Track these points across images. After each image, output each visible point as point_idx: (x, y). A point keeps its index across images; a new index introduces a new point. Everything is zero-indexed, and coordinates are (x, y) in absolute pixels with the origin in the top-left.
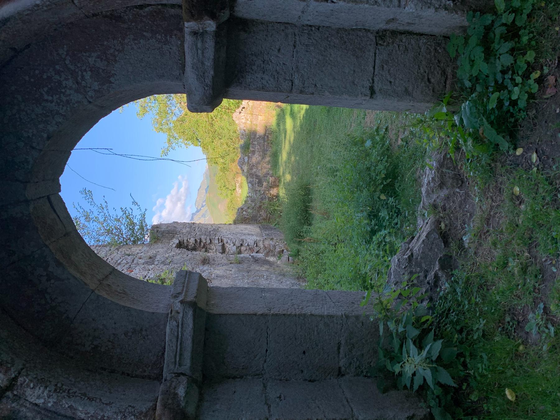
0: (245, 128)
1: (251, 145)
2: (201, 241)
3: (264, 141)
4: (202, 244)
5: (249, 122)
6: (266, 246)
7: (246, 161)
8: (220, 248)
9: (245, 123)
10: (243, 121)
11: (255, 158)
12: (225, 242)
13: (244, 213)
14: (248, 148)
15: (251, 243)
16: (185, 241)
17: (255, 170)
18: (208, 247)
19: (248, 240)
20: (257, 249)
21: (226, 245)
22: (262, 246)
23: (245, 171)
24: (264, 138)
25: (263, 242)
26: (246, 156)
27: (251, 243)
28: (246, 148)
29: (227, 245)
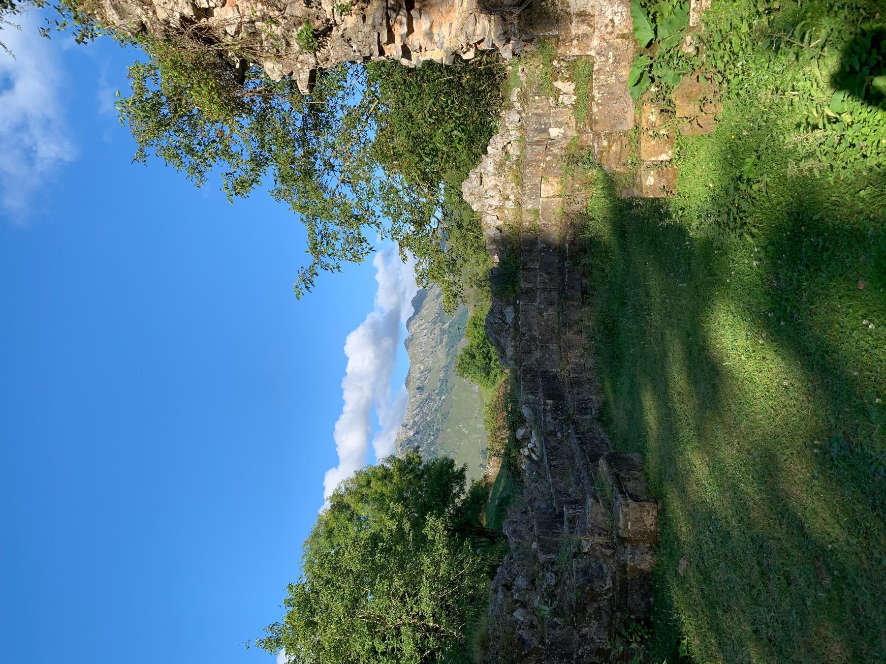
1: (521, 274)
7: (510, 319)
13: (519, 614)
14: (514, 283)
17: (537, 354)
26: (509, 304)
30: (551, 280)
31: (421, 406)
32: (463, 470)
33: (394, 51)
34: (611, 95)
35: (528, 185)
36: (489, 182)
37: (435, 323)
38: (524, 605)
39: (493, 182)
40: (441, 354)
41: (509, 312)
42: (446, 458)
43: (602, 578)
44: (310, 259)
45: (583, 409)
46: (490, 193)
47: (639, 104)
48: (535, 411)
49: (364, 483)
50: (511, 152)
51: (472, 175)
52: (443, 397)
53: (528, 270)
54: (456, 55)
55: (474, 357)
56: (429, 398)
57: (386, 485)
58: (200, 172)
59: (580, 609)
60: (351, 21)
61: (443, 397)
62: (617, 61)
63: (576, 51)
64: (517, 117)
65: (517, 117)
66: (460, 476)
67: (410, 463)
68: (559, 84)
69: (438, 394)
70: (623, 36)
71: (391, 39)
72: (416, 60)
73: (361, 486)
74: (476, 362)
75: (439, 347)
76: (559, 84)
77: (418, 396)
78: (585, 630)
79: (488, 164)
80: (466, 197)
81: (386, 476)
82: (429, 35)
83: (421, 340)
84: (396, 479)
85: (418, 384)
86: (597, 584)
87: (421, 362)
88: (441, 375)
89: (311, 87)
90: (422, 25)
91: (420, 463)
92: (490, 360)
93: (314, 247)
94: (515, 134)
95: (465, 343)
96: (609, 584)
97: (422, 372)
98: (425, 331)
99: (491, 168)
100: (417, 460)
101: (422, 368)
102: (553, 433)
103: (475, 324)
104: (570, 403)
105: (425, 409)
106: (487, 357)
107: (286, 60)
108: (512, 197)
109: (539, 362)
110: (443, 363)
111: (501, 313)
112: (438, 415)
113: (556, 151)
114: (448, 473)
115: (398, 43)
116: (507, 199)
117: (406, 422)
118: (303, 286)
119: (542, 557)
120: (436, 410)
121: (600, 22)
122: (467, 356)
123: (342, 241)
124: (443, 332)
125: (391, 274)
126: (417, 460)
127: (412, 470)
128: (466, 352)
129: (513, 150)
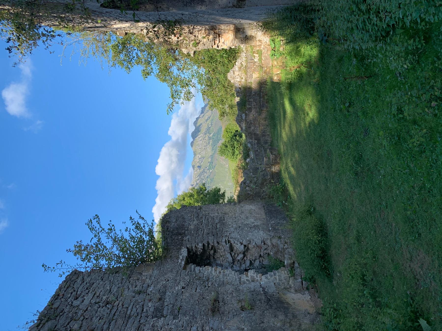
0: (240, 86)
1: (247, 103)
2: (208, 244)
3: (260, 98)
4: (210, 247)
5: (243, 80)
6: (274, 243)
7: (244, 118)
8: (228, 249)
9: (240, 82)
10: (238, 80)
11: (253, 115)
12: (232, 242)
13: (247, 188)
14: (245, 106)
15: (259, 242)
16: (193, 248)
17: (253, 128)
18: (216, 248)
19: (255, 240)
20: (265, 247)
21: (234, 245)
22: (270, 244)
23: (244, 128)
24: (259, 95)
25: (271, 240)
26: (243, 113)
27: (259, 242)
28: (242, 105)
29: (235, 245)
30: (257, 105)
31: (200, 175)
32: (224, 193)
33: (215, 47)
34: (266, 59)
35: (249, 74)
36: (237, 73)
37: (205, 134)
38: (248, 186)
39: (238, 73)
40: (209, 149)
41: (243, 115)
42: (217, 188)
43: (267, 175)
44: (171, 100)
45: (266, 143)
46: (237, 77)
47: (272, 61)
48: (252, 145)
49: (182, 199)
50: (243, 64)
51: (231, 71)
52: (211, 171)
53: (249, 101)
54: (231, 48)
55: (227, 147)
56: (204, 171)
57: (191, 199)
58: (129, 68)
59: (262, 184)
60: (205, 40)
61: (211, 171)
62: (267, 51)
63: (258, 49)
64: (245, 54)
65: (245, 54)
66: (223, 195)
67: (201, 190)
68: (255, 55)
69: (208, 169)
70: (269, 45)
71: (215, 44)
72: (220, 48)
73: (181, 200)
74: (227, 149)
75: (208, 146)
76: (255, 55)
77: (198, 170)
78: (264, 189)
79: (236, 68)
80: (229, 78)
81: (191, 196)
82: (224, 43)
83: (199, 143)
84: (196, 196)
85: (198, 164)
86: (266, 177)
87: (199, 154)
88: (210, 160)
89: (194, 55)
90: (222, 40)
91: (206, 190)
92: (234, 148)
93: (173, 96)
94: (244, 59)
95: (223, 141)
96: (269, 177)
97: (200, 159)
98: (201, 138)
99: (237, 69)
100: (204, 188)
101: (200, 156)
102: (257, 151)
103: (227, 132)
104: (262, 142)
105: (202, 177)
106: (233, 146)
107: (188, 49)
108: (244, 78)
109: (253, 130)
110: (210, 154)
111: (241, 116)
112: (209, 180)
113: (257, 64)
114: (217, 193)
115: (216, 45)
116: (242, 79)
117: (193, 183)
118: (169, 110)
119: (253, 176)
120: (207, 177)
121: (263, 42)
122: (224, 146)
123: (183, 94)
124: (210, 138)
125: (192, 107)
126: (204, 188)
127: (202, 193)
128: (223, 144)
129: (244, 64)
